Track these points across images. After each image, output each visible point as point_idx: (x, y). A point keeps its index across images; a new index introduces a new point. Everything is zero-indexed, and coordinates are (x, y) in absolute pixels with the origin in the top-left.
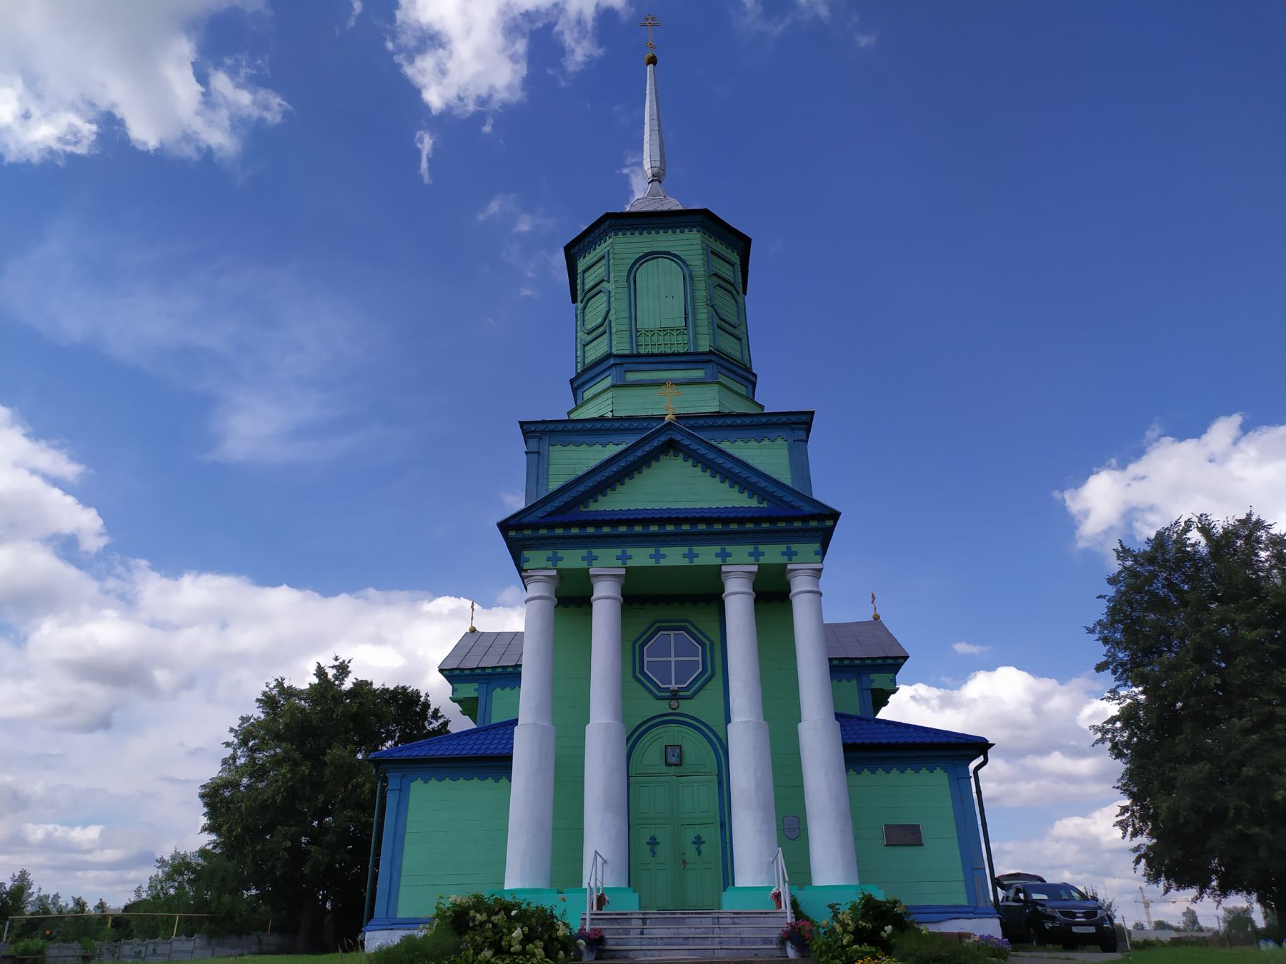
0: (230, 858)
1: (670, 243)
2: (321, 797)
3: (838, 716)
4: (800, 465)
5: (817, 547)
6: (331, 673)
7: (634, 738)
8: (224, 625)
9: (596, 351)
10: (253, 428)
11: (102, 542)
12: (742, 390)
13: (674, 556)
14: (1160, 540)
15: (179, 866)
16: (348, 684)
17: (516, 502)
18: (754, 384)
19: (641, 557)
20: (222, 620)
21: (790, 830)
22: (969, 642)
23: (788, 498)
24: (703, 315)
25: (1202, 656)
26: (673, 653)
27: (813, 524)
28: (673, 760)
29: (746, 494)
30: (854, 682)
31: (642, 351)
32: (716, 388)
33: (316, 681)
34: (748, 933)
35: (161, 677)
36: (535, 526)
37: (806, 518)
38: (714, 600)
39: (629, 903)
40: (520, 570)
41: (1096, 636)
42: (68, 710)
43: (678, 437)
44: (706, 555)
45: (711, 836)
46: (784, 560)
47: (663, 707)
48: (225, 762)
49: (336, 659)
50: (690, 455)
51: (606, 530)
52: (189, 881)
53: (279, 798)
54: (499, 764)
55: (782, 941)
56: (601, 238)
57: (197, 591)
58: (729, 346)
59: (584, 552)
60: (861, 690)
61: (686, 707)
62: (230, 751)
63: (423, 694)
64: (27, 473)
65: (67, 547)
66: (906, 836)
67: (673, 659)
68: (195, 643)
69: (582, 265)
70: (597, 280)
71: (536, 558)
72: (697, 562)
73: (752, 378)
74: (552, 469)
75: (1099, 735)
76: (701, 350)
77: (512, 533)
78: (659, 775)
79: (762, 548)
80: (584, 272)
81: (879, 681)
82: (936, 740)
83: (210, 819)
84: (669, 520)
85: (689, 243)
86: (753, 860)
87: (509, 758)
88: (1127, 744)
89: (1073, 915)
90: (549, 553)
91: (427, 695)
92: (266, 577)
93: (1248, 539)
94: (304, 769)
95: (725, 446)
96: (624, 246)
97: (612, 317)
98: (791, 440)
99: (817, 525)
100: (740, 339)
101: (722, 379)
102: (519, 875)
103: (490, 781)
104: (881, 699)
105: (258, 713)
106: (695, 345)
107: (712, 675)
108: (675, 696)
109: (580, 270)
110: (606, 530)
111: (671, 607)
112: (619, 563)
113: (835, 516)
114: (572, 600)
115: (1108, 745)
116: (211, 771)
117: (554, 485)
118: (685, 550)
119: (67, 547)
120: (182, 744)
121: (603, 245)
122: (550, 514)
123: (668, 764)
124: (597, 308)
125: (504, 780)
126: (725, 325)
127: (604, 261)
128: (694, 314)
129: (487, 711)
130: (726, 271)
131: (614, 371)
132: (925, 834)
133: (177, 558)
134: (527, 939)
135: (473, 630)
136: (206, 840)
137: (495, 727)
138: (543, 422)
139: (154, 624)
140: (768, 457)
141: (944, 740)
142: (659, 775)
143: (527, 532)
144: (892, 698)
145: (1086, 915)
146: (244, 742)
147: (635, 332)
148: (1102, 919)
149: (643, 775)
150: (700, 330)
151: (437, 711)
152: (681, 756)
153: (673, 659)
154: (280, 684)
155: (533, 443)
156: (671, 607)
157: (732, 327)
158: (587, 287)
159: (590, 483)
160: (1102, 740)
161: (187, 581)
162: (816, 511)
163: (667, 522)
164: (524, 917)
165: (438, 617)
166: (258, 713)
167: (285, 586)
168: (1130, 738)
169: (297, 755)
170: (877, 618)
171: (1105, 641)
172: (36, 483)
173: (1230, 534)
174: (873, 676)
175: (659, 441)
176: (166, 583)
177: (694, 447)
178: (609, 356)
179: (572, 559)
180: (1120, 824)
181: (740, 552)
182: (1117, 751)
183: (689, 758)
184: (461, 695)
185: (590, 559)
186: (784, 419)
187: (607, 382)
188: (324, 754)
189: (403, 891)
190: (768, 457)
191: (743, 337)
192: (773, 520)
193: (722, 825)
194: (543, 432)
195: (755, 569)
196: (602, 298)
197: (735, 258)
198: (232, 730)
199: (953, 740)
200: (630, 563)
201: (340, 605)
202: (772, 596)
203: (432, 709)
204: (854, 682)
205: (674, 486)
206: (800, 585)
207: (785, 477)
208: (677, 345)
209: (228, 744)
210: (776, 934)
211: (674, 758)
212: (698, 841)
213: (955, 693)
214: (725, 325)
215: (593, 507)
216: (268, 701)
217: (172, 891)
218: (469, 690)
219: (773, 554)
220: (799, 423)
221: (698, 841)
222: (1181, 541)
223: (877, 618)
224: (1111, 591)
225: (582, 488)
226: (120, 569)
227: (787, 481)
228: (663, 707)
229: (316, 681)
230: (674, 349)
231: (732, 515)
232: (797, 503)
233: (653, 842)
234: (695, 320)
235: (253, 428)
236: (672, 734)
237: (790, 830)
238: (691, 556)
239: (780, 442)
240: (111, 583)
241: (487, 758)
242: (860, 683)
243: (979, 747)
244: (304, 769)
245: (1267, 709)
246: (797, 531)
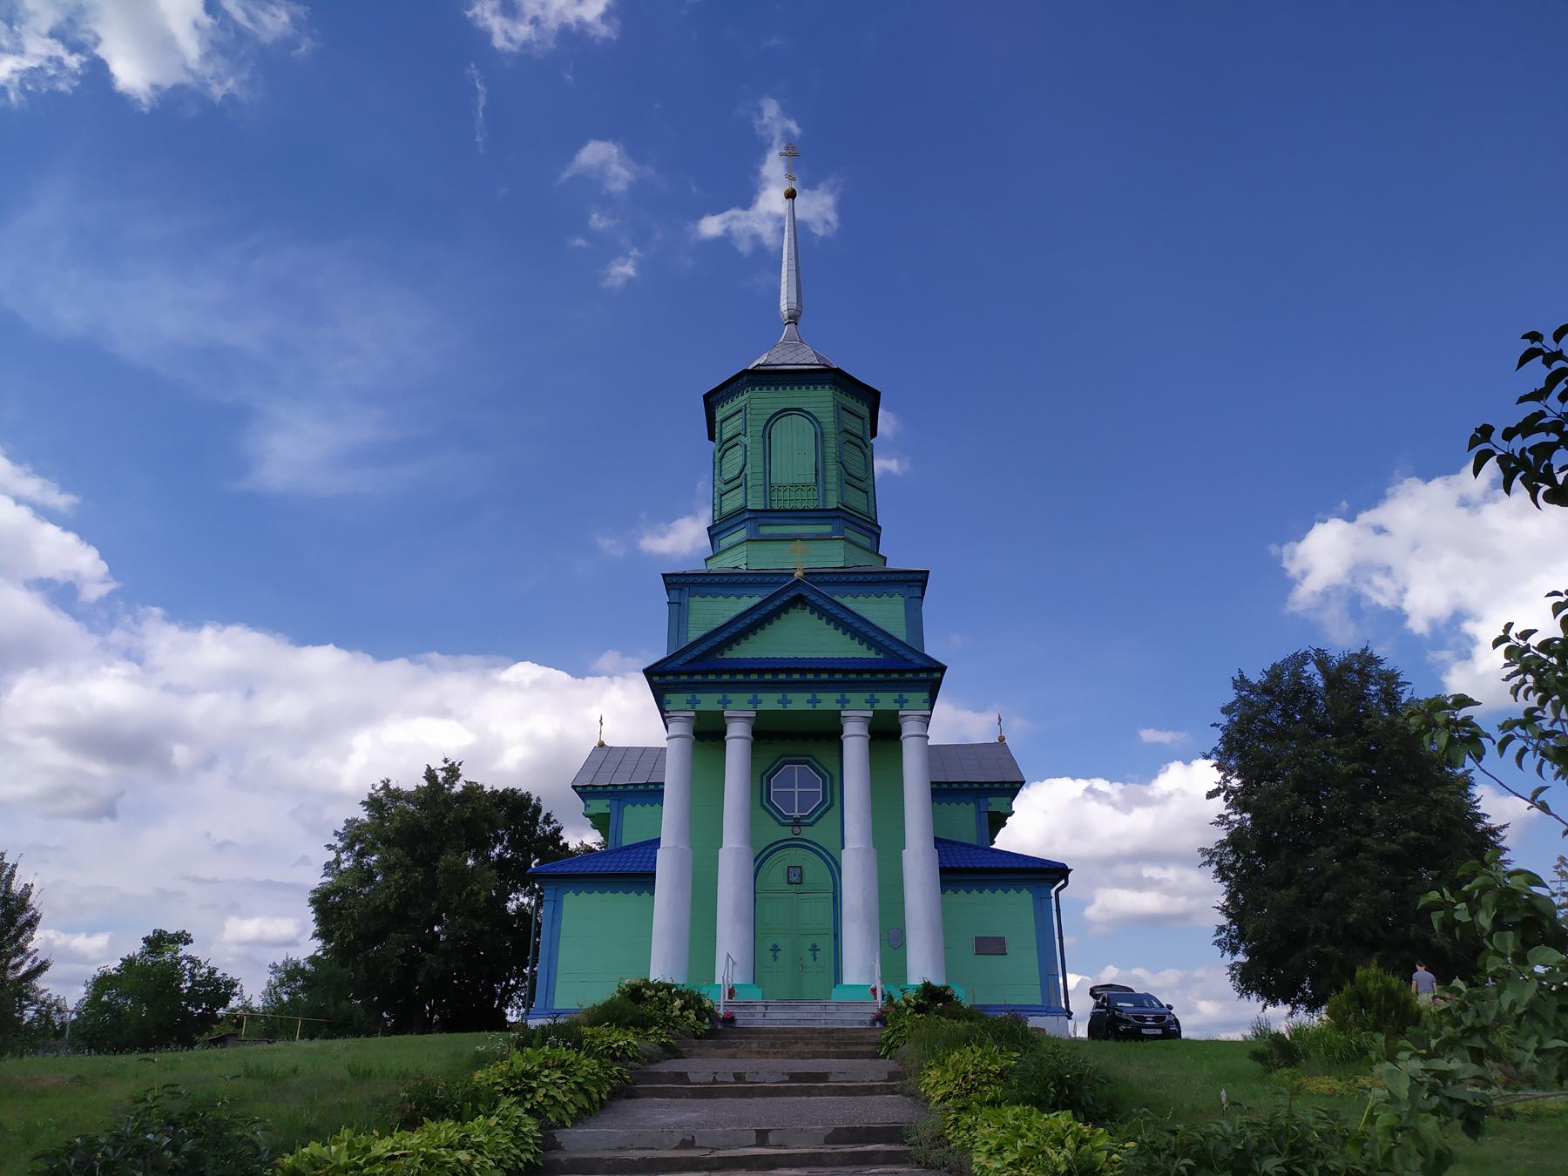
0: (343, 965)
2: (435, 905)
3: (938, 842)
4: (915, 622)
5: (925, 695)
6: (441, 775)
7: (760, 860)
8: (250, 693)
9: (733, 502)
10: (296, 449)
11: (104, 589)
12: (865, 541)
13: (799, 702)
14: (1275, 673)
15: (292, 973)
16: (458, 787)
17: (658, 653)
18: (878, 536)
19: (770, 702)
20: (247, 685)
21: (892, 939)
22: (1158, 728)
23: (902, 652)
24: (832, 472)
25: (1301, 786)
26: (796, 784)
27: (923, 675)
28: (794, 879)
29: (864, 647)
31: (775, 507)
32: (842, 543)
33: (425, 784)
34: (847, 1017)
35: (181, 754)
36: (677, 673)
37: (916, 671)
38: (832, 735)
39: (755, 995)
40: (662, 711)
41: (1212, 762)
42: (64, 792)
43: (806, 594)
44: (828, 701)
45: (826, 944)
46: (897, 706)
47: (786, 833)
48: (328, 865)
49: (446, 761)
50: (816, 609)
51: (740, 677)
52: (303, 988)
53: (391, 905)
54: (644, 880)
55: (873, 1022)
56: (740, 390)
57: (218, 649)
58: (856, 500)
59: (719, 696)
60: (979, 813)
61: (807, 833)
62: (332, 856)
63: (534, 798)
64: (12, 502)
65: (62, 594)
66: (991, 946)
67: (796, 790)
68: (208, 711)
69: (720, 414)
70: (734, 432)
71: (677, 700)
72: (819, 707)
74: (692, 619)
75: (1207, 858)
76: (830, 506)
77: (656, 679)
78: (782, 891)
79: (877, 696)
81: (995, 804)
82: (1023, 865)
84: (796, 670)
85: (821, 400)
86: (859, 964)
87: (654, 875)
88: (1232, 868)
89: (1145, 1019)
90: (688, 696)
91: (538, 799)
92: (306, 634)
93: (1360, 672)
94: (418, 875)
96: (763, 401)
97: (748, 471)
99: (927, 678)
101: (849, 533)
102: (659, 971)
103: (633, 895)
104: (998, 821)
105: (363, 815)
106: (824, 502)
107: (831, 805)
108: (797, 823)
109: (718, 418)
110: (740, 677)
111: (796, 743)
112: (751, 707)
113: (942, 669)
114: (708, 735)
115: (1214, 867)
116: (316, 878)
117: (694, 635)
118: (809, 696)
119: (62, 594)
120: (208, 835)
121: (741, 398)
122: (690, 661)
123: (790, 883)
124: (734, 459)
125: (646, 895)
126: (853, 481)
127: (741, 415)
128: (824, 470)
129: (619, 827)
130: (856, 426)
131: (748, 524)
132: (1009, 947)
133: (195, 606)
134: (683, 1009)
135: (602, 745)
136: (313, 947)
137: (628, 848)
138: (683, 575)
139: (167, 688)
140: (884, 612)
141: (1031, 865)
142: (782, 891)
143: (670, 678)
144: (1009, 820)
145: (1155, 1019)
146: (350, 847)
147: (769, 487)
148: (1170, 1022)
149: (768, 891)
150: (829, 487)
151: (548, 815)
152: (801, 875)
153: (796, 790)
154: (386, 785)
155: (675, 593)
156: (796, 743)
157: (861, 480)
158: (725, 437)
159: (726, 635)
160: (1210, 863)
161: (208, 634)
162: (925, 664)
163: (796, 669)
164: (679, 994)
165: (518, 687)
166: (363, 815)
167: (331, 646)
168: (1237, 861)
169: (408, 861)
170: (1002, 739)
171: (1219, 767)
172: (23, 513)
173: (1346, 667)
174: (990, 800)
175: (790, 595)
176: (186, 636)
177: (820, 602)
178: (744, 509)
179: (709, 702)
180: (1218, 943)
181: (858, 698)
182: (1222, 873)
183: (807, 878)
184: (592, 811)
185: (725, 702)
186: (902, 577)
187: (741, 534)
188: (437, 860)
189: (558, 986)
190: (884, 612)
191: (870, 489)
192: (887, 672)
193: (836, 936)
194: (684, 584)
196: (738, 451)
197: (864, 411)
198: (336, 833)
199: (1038, 865)
200: (760, 707)
201: (398, 669)
202: (885, 735)
203: (543, 814)
205: (801, 637)
206: (910, 728)
207: (901, 634)
208: (807, 501)
209: (330, 847)
210: (868, 1018)
211: (795, 877)
212: (814, 949)
213: (1144, 788)
214: (853, 481)
215: (728, 655)
216: (373, 804)
217: (285, 998)
218: (601, 806)
219: (886, 701)
220: (915, 582)
221: (814, 949)
222: (1296, 675)
223: (1002, 739)
224: (1224, 720)
225: (718, 639)
226: (128, 619)
227: (903, 637)
228: (786, 833)
229: (425, 784)
230: (805, 505)
231: (851, 667)
232: (909, 656)
233: (775, 949)
234: (824, 476)
235: (296, 449)
236: (795, 856)
237: (892, 939)
238: (814, 701)
239: (897, 598)
240: (117, 636)
241: (627, 871)
242: (978, 806)
243: (1055, 873)
244: (418, 875)
245: (1353, 839)
246: (909, 681)
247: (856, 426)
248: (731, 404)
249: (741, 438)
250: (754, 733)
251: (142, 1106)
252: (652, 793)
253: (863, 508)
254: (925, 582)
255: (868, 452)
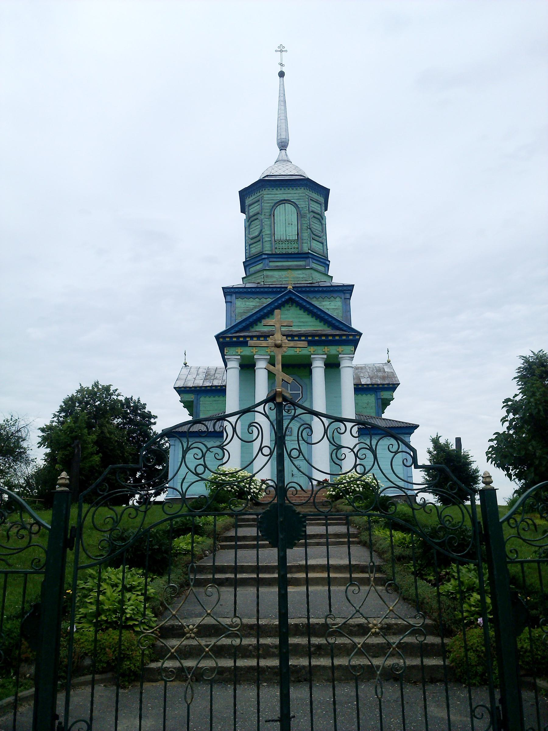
1: (290, 195)
30: (374, 395)
69: (248, 202)
73: (327, 263)
80: (250, 205)
81: (385, 395)
83: (48, 463)
95: (316, 303)
98: (343, 298)
100: (323, 243)
104: (386, 403)
113: (360, 334)
114: (247, 367)
130: (315, 207)
137: (384, 419)
144: (391, 402)
155: (228, 298)
181: (320, 349)
195: (325, 356)
202: (333, 366)
204: (374, 395)
206: (344, 363)
218: (190, 397)
247: (315, 207)
248: (253, 197)
249: (258, 216)
250: (240, 366)
251: (404, 541)
252: (221, 391)
253: (321, 252)
254: (352, 291)
255: (324, 222)
